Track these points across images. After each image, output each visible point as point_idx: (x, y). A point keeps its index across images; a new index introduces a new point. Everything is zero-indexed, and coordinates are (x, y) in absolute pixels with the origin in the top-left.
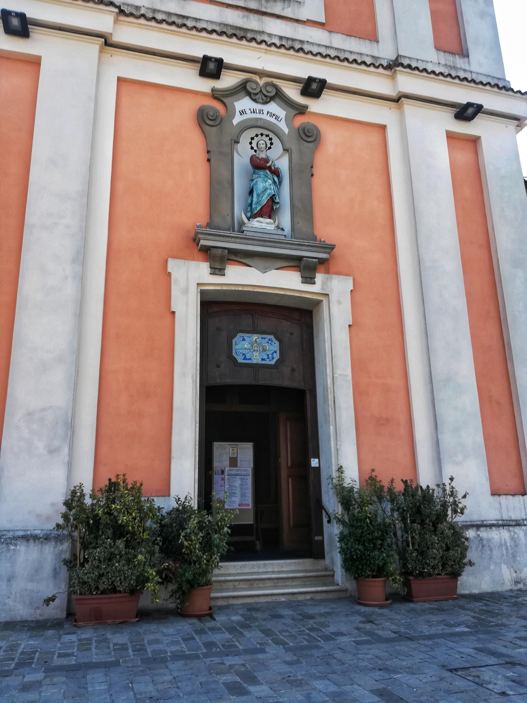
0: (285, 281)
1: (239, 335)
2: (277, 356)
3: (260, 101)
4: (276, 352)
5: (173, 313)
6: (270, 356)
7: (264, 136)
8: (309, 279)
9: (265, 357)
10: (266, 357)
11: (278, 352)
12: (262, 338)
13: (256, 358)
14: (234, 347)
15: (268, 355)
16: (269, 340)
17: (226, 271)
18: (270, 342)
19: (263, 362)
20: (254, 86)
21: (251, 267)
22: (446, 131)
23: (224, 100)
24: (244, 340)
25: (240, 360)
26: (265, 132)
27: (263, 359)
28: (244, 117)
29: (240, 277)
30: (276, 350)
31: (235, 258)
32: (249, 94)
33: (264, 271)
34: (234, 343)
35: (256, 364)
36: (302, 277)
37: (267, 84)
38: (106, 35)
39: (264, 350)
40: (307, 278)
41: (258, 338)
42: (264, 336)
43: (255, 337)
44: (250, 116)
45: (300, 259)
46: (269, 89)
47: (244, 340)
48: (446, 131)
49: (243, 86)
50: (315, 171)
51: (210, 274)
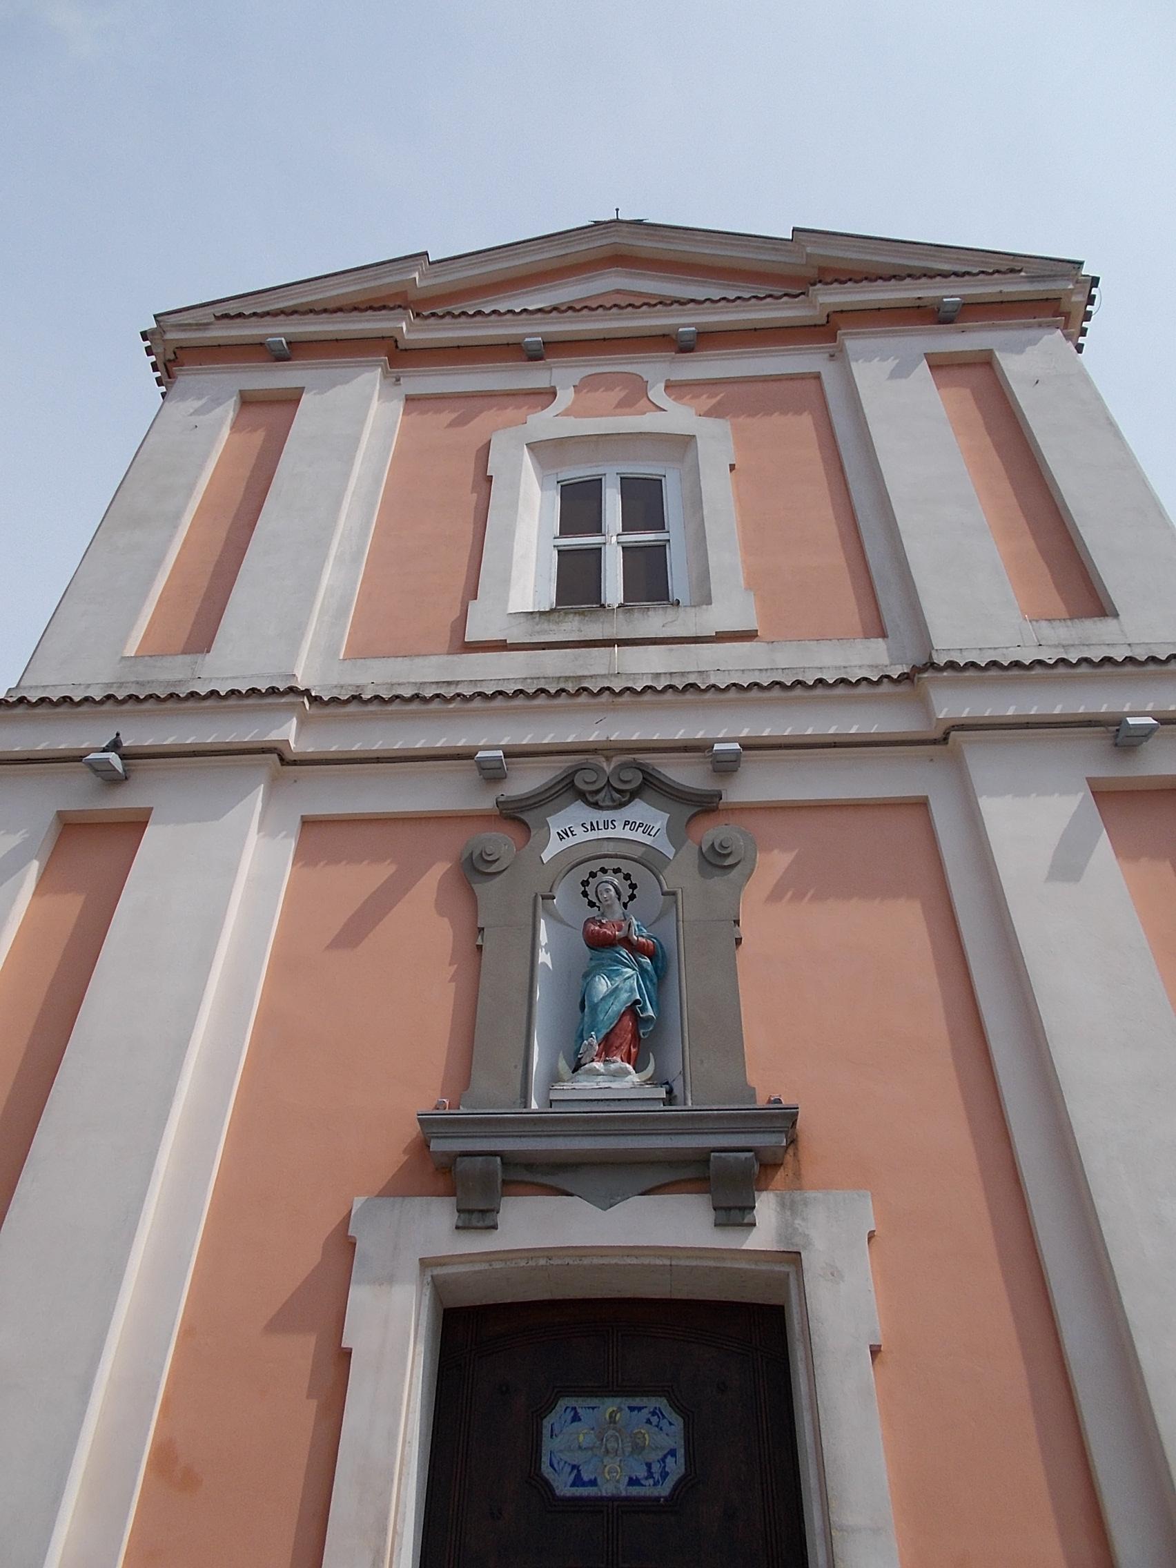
0: (662, 1229)
1: (563, 1403)
2: (676, 1467)
3: (608, 803)
4: (672, 1453)
5: (348, 1353)
6: (656, 1468)
7: (610, 872)
8: (735, 1213)
9: (641, 1473)
10: (641, 1473)
11: (681, 1452)
12: (632, 1409)
13: (612, 1479)
14: (548, 1445)
15: (649, 1465)
16: (653, 1413)
17: (500, 1218)
18: (654, 1420)
19: (635, 1491)
20: (590, 776)
21: (572, 1195)
22: (1087, 779)
23: (524, 817)
24: (576, 1418)
25: (563, 1486)
26: (615, 863)
27: (633, 1482)
28: (570, 842)
29: (545, 1230)
30: (673, 1445)
31: (528, 1177)
32: (582, 796)
33: (606, 1201)
34: (546, 1432)
35: (612, 1499)
36: (458, 1211)
37: (623, 766)
38: (279, 746)
39: (638, 1448)
40: (730, 1209)
41: (620, 1409)
42: (637, 1402)
43: (610, 1406)
44: (581, 836)
45: (701, 1159)
46: (627, 775)
47: (576, 1418)
48: (1087, 779)
49: (568, 781)
50: (744, 931)
51: (457, 1228)
